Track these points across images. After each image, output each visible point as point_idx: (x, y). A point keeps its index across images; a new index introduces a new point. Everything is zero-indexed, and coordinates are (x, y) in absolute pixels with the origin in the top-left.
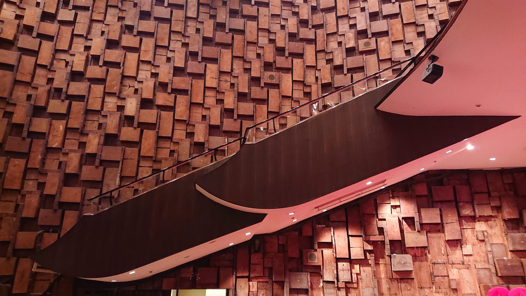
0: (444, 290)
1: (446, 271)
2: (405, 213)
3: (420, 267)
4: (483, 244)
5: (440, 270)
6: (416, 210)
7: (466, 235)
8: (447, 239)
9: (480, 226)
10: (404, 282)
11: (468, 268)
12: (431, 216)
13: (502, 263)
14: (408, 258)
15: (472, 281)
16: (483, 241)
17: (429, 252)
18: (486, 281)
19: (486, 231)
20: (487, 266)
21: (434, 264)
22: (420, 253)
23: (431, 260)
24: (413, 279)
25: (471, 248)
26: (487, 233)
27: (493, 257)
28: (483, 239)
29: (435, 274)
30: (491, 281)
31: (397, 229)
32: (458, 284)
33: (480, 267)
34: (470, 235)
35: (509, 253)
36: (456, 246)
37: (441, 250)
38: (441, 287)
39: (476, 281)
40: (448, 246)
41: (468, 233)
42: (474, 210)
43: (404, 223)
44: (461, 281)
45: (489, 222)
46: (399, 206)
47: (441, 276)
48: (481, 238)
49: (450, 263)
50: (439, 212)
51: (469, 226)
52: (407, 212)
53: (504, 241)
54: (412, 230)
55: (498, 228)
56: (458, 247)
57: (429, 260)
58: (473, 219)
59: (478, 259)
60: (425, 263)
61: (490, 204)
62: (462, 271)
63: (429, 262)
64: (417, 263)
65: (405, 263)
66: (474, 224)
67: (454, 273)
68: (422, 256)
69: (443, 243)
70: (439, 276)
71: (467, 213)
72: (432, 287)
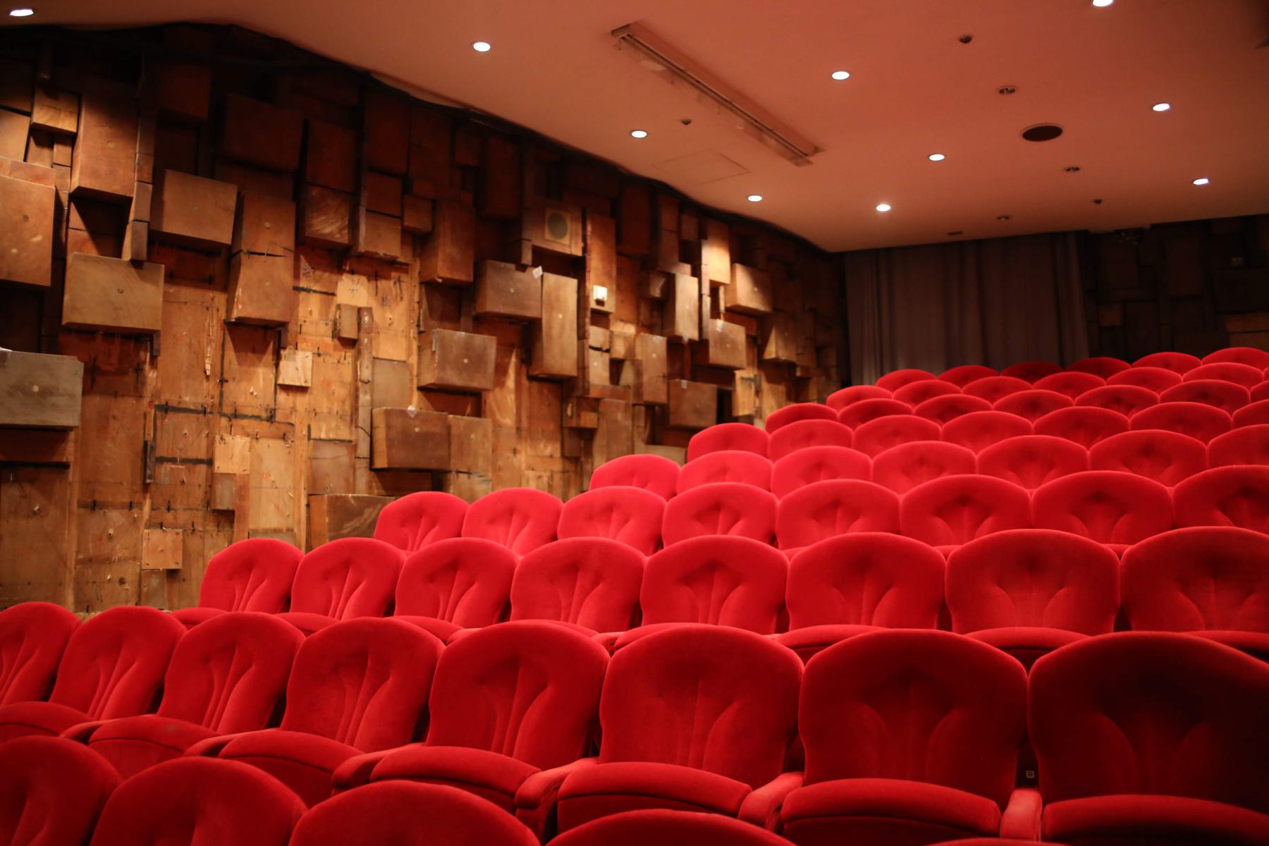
0: (184, 517)
1: (204, 443)
2: (95, 174)
3: (103, 423)
4: (350, 354)
5: (183, 436)
6: (148, 169)
7: (302, 312)
8: (236, 314)
9: (353, 291)
10: (16, 481)
11: (284, 437)
12: (200, 212)
13: (397, 422)
14: (67, 371)
15: (289, 483)
16: (350, 343)
17: (154, 359)
18: (334, 485)
19: (370, 310)
20: (344, 434)
21: (166, 409)
22: (118, 355)
23: (157, 394)
24: (66, 466)
25: (309, 364)
26: (372, 317)
27: (372, 404)
28: (353, 336)
29: (162, 451)
30: (351, 487)
31: (41, 237)
32: (243, 491)
33: (323, 436)
34: (316, 315)
35: (416, 395)
36: (259, 351)
37: (204, 357)
38: (178, 505)
39: (303, 485)
40: (229, 345)
41: (310, 311)
42: (353, 227)
43: (75, 219)
44: (253, 483)
45: (383, 284)
46: (70, 139)
47: (184, 461)
48: (349, 331)
49: (227, 410)
50: (232, 202)
51: (316, 281)
52: (103, 168)
53: (409, 355)
54: (102, 251)
55: (402, 307)
56: (264, 352)
57: (148, 391)
58: (339, 258)
59: (324, 406)
60: (128, 403)
61: (401, 218)
62: (264, 443)
63: (146, 401)
64: (96, 401)
65: (46, 392)
66: (334, 277)
67: (234, 452)
68: (121, 372)
69: (215, 330)
70: (173, 460)
71: (327, 230)
72: (140, 506)
